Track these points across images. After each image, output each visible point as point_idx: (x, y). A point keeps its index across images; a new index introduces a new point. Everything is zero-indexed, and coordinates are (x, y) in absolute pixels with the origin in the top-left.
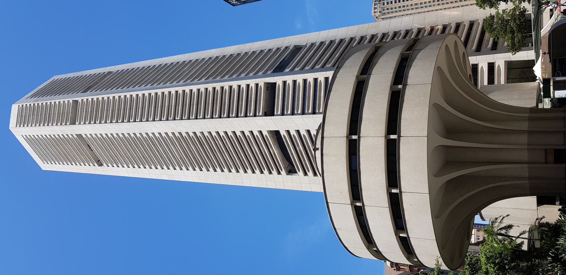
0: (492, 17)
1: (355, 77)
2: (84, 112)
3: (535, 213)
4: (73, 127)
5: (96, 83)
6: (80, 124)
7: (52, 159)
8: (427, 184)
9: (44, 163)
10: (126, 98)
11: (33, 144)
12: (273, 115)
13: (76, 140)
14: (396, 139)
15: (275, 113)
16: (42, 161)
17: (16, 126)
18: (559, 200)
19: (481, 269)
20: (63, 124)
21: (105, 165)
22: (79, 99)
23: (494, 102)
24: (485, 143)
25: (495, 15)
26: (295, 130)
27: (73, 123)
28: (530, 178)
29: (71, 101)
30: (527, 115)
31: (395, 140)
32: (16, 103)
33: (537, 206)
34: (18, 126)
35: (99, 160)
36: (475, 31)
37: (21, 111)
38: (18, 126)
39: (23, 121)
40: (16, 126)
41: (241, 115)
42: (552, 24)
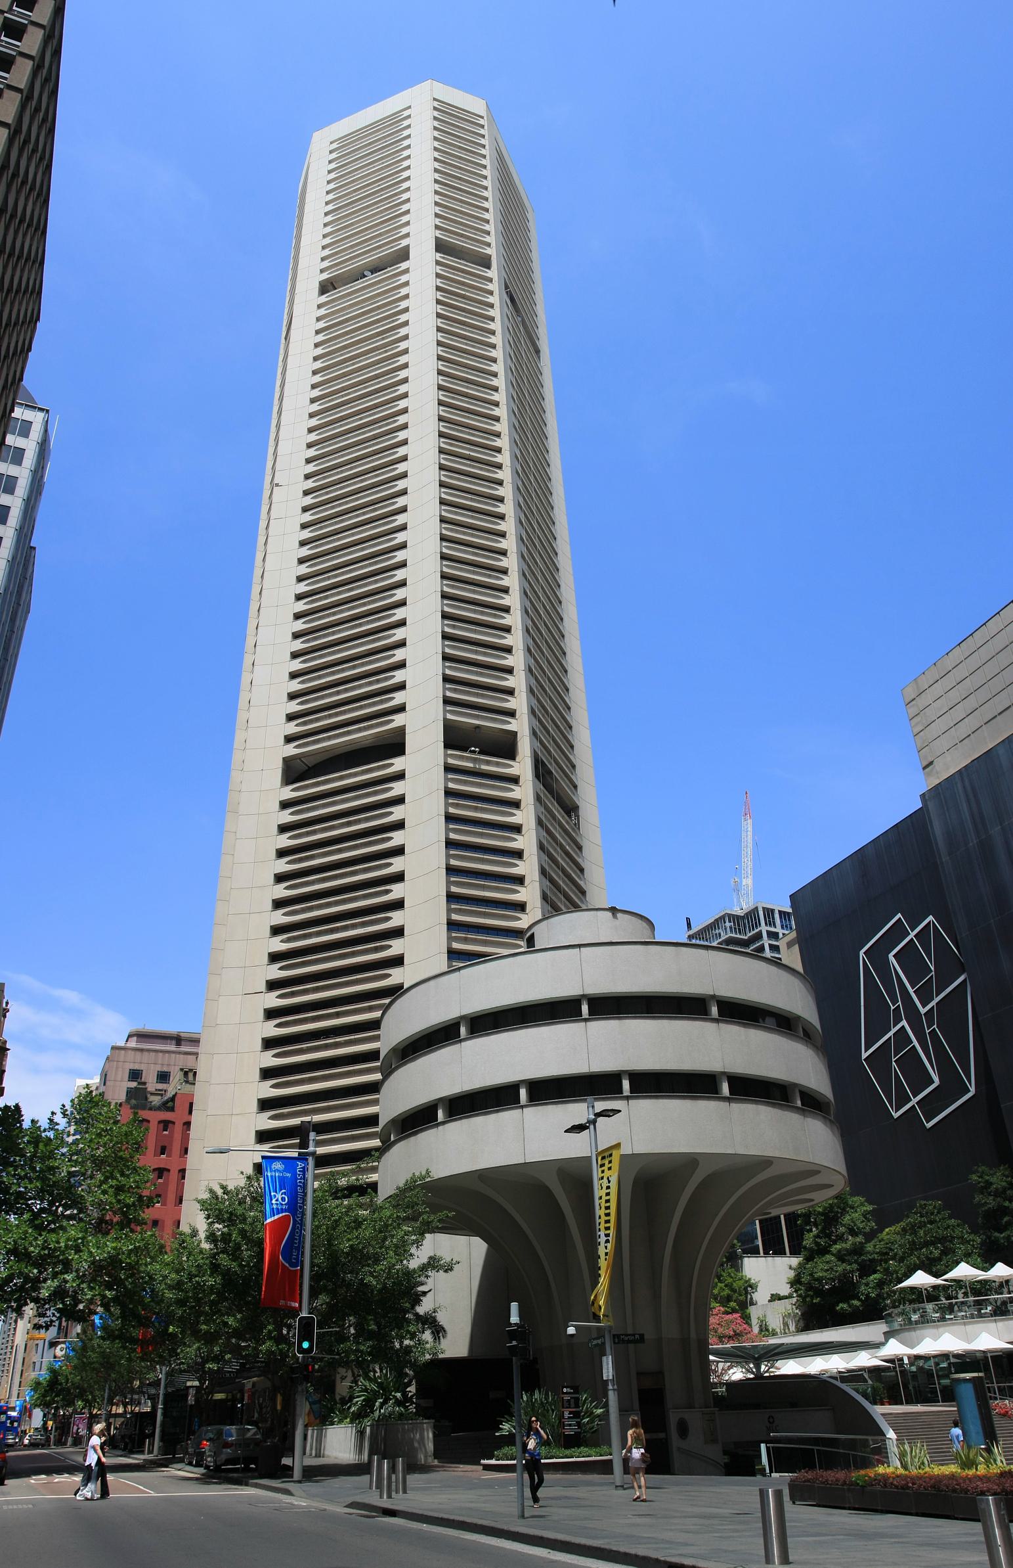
1: (712, 993)
2: (729, 947)
7: (336, 253)
8: (928, 787)
9: (331, 143)
10: (487, 306)
12: (447, 745)
14: (621, 1092)
15: (450, 752)
16: (340, 139)
17: (435, 99)
18: (636, 1405)
19: (95, 1267)
21: (404, 243)
22: (493, 273)
26: (405, 703)
27: (441, 246)
30: (693, 1335)
31: (620, 1091)
34: (436, 104)
35: (336, 289)
37: (470, 119)
38: (436, 104)
39: (448, 118)
41: (444, 510)
42: (752, 1411)
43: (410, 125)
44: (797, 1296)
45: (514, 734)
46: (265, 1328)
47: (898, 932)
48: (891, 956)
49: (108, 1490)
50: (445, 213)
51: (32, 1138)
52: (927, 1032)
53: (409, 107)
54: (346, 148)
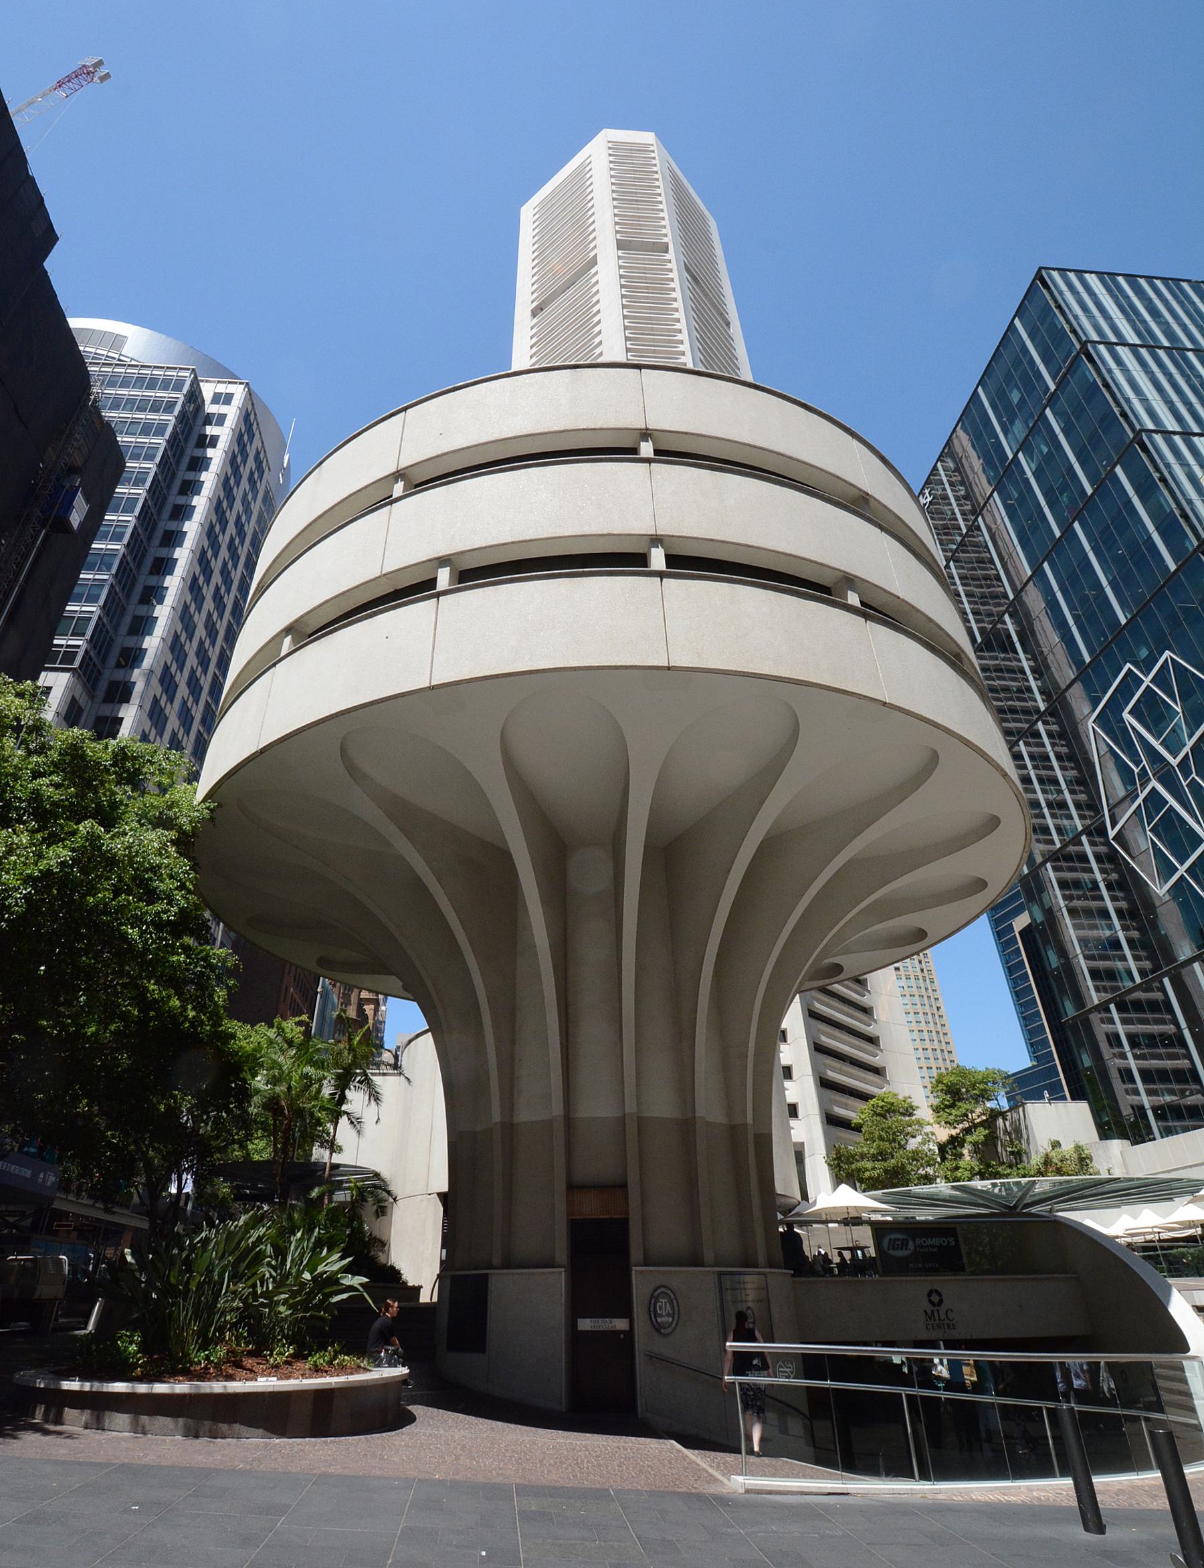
0: (909, 1111)
3: (420, 1189)
4: (613, 245)
5: (706, 295)
6: (619, 258)
7: (541, 339)
11: (574, 239)
13: (586, 302)
17: (609, 142)
18: (562, 1255)
20: (618, 228)
22: (671, 255)
23: (790, 998)
24: (640, 968)
25: (914, 1118)
27: (620, 245)
28: (509, 1128)
29: (665, 240)
32: (658, 141)
33: (439, 1194)
36: (865, 1078)
37: (643, 149)
39: (619, 153)
40: (609, 142)
43: (600, 320)
44: (746, 1301)
45: (668, 243)
46: (29, 1147)
47: (1131, 682)
48: (1126, 716)
49: (173, 508)
50: (622, 221)
51: (292, 1101)
52: (1184, 784)
53: (925, 1311)
54: (546, 211)
